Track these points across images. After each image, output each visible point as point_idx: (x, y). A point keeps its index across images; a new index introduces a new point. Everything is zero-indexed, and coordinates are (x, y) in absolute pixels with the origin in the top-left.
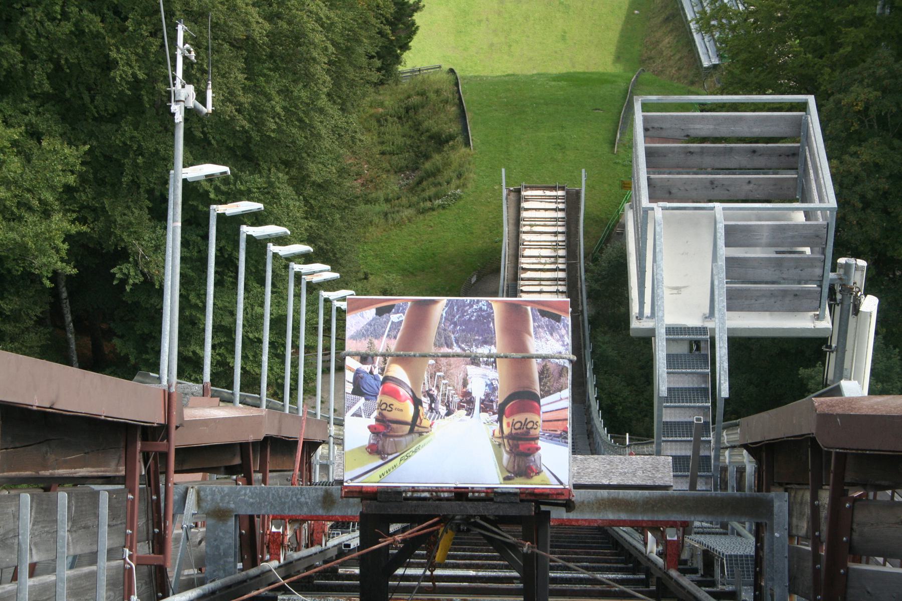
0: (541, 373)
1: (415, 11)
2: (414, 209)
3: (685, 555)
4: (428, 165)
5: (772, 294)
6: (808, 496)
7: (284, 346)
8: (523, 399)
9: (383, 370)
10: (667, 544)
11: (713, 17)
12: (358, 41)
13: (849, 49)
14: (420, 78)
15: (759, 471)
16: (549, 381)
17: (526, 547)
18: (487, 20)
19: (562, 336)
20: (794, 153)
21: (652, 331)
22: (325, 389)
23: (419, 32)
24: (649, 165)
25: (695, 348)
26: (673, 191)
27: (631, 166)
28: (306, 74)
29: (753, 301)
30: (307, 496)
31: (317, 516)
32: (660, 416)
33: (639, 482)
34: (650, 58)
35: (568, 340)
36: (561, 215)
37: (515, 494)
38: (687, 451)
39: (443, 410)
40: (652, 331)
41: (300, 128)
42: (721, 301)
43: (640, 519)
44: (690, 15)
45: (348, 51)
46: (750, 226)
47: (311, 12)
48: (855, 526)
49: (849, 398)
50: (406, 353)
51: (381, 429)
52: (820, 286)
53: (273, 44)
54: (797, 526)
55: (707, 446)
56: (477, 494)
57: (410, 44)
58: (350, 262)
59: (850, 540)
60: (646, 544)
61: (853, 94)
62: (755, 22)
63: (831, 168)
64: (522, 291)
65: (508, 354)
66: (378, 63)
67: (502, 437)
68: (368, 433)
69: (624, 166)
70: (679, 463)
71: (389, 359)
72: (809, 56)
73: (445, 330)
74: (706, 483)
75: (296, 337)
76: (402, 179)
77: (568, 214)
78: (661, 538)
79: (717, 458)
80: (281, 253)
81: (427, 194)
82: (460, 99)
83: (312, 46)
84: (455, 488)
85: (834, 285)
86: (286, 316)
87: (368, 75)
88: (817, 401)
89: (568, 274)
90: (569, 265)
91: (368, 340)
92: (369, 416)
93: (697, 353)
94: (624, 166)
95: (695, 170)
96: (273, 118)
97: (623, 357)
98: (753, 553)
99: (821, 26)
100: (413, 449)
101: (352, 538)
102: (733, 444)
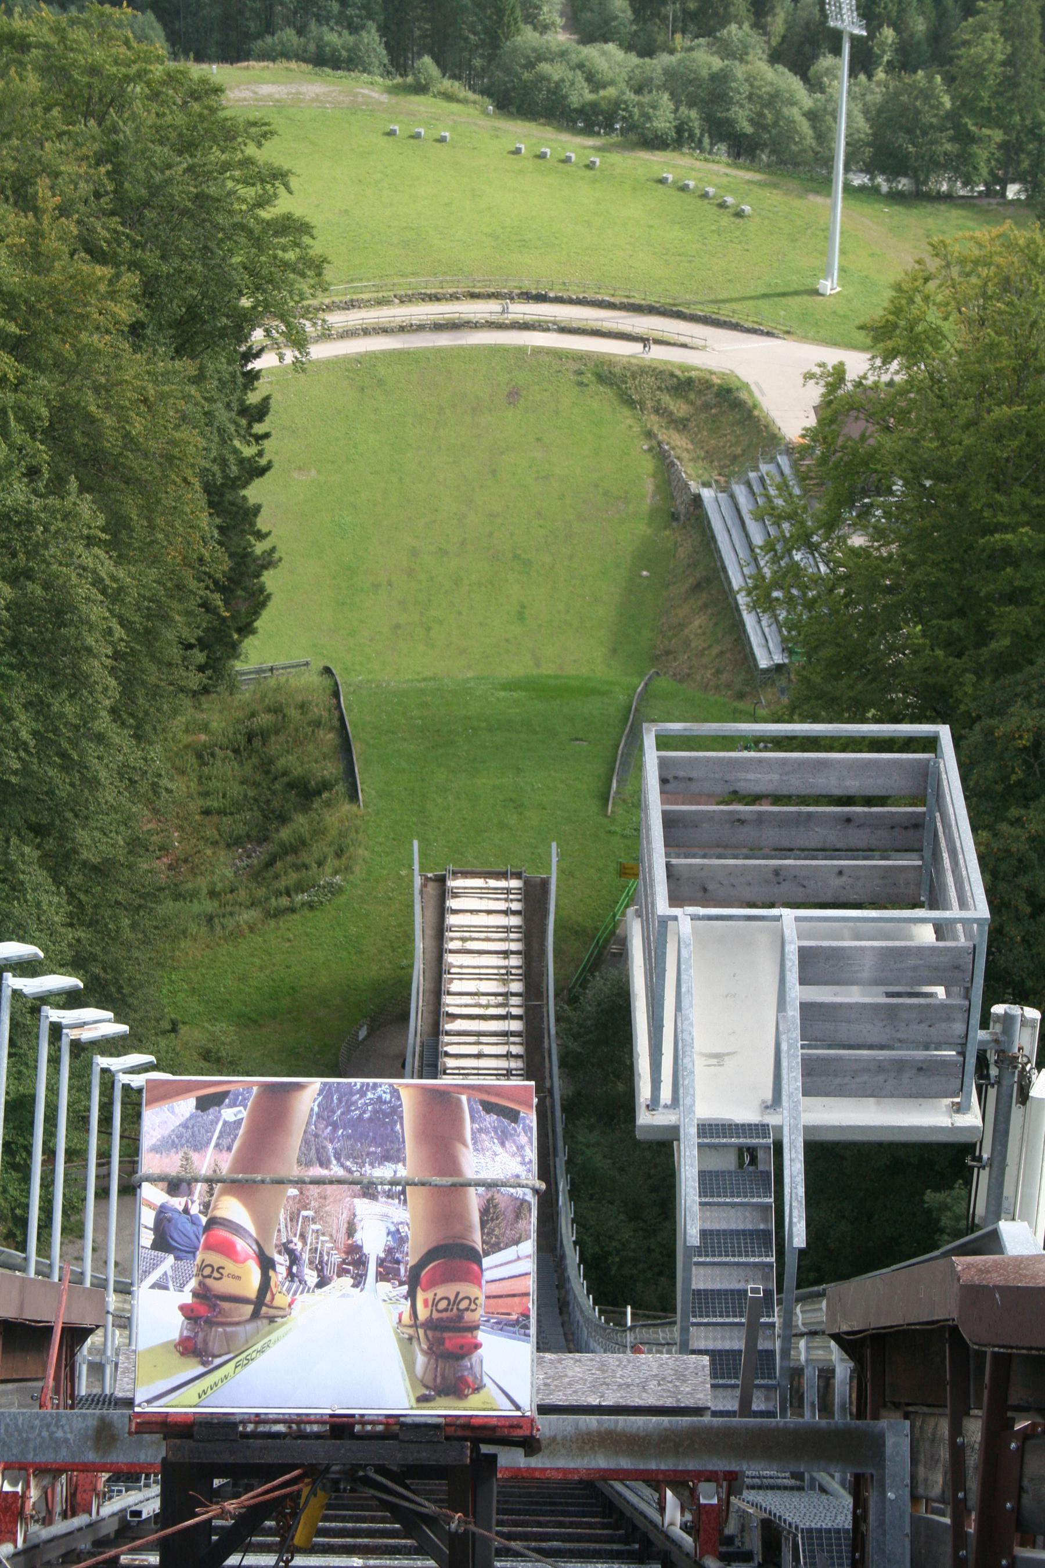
0: (485, 1212)
1: (265, 567)
2: (259, 910)
3: (731, 1528)
4: (285, 833)
5: (880, 1067)
6: (944, 1427)
7: (28, 1150)
8: (451, 1257)
9: (206, 1206)
10: (700, 1511)
11: (776, 585)
12: (166, 618)
13: (1007, 642)
14: (272, 682)
15: (858, 1374)
16: (498, 1226)
17: (456, 1522)
18: (390, 584)
19: (520, 1148)
20: (917, 824)
21: (675, 1130)
22: (101, 1228)
23: (271, 604)
24: (669, 842)
25: (747, 1161)
26: (710, 887)
27: (638, 837)
28: (74, 675)
29: (847, 1080)
30: (67, 1428)
31: (85, 1464)
32: (688, 1280)
33: (651, 1401)
34: (668, 653)
35: (532, 1154)
36: (515, 921)
37: (436, 1427)
38: (736, 1342)
39: (311, 1277)
40: (675, 1130)
41: (64, 768)
42: (793, 1080)
43: (654, 1467)
44: (736, 581)
45: (148, 636)
46: (843, 949)
47: (84, 569)
48: (1026, 1483)
49: (1016, 1258)
50: (248, 1176)
51: (203, 1310)
52: (962, 1054)
53: (18, 621)
54: (926, 1480)
55: (768, 1332)
56: (369, 1428)
57: (256, 624)
58: (146, 1002)
59: (1018, 1508)
60: (662, 1509)
61: (1013, 719)
62: (846, 595)
63: (977, 844)
64: (447, 1054)
65: (427, 1178)
66: (200, 657)
67: (415, 1326)
68: (179, 1318)
69: (624, 837)
70: (722, 1363)
71: (218, 1187)
72: (940, 653)
73: (316, 1136)
74: (767, 1399)
75: (50, 1133)
76: (240, 858)
77: (526, 920)
78: (689, 1499)
79: (786, 1353)
80: (26, 991)
81: (282, 883)
82: (342, 719)
83: (86, 628)
84: (331, 1416)
85: (985, 1051)
86: (33, 1098)
87: (182, 678)
88: (960, 1262)
89: (527, 1024)
90: (528, 1008)
91: (181, 1154)
92: (181, 1288)
93: (751, 1168)
94: (624, 837)
95: (745, 851)
96: (16, 750)
97: (622, 1170)
98: (848, 1525)
99: (960, 602)
100: (258, 1346)
101: (147, 1499)
102: (813, 1328)
